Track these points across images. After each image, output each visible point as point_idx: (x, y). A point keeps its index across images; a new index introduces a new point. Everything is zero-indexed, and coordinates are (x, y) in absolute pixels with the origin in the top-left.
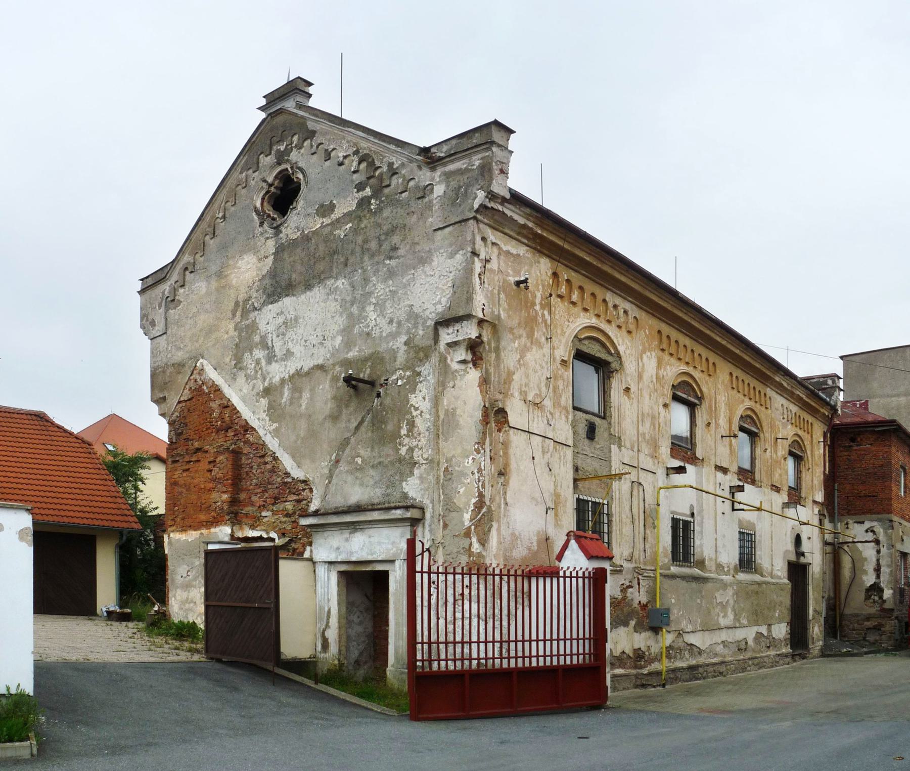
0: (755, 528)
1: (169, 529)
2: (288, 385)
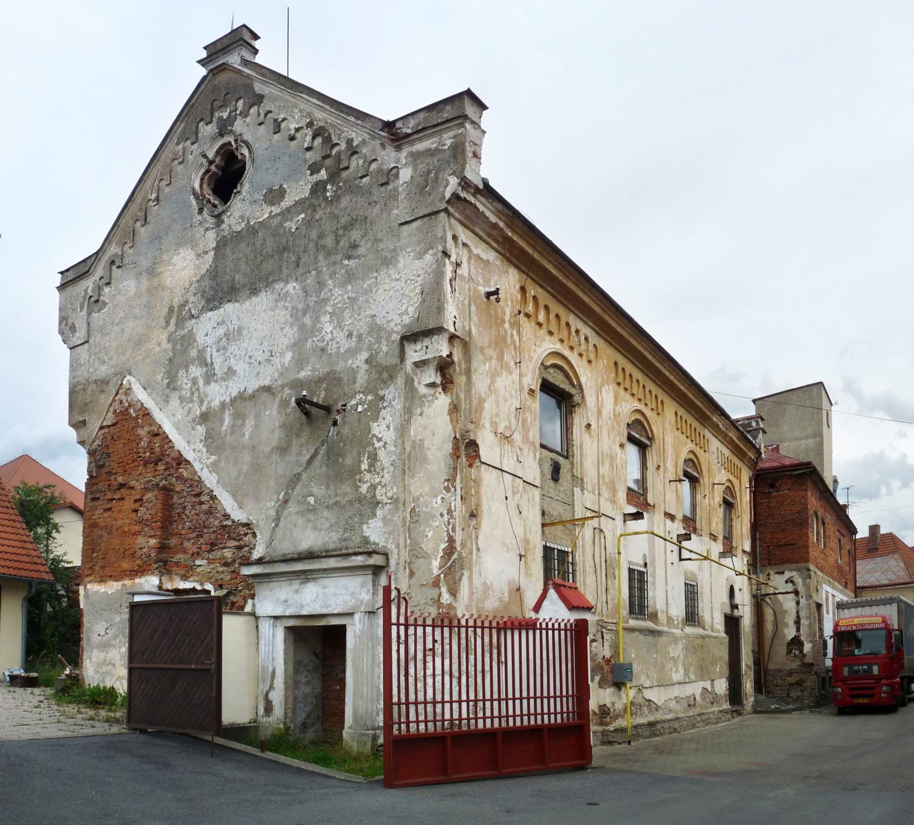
0: (696, 578)
1: (86, 579)
2: (230, 410)
